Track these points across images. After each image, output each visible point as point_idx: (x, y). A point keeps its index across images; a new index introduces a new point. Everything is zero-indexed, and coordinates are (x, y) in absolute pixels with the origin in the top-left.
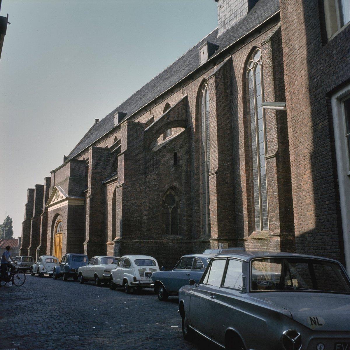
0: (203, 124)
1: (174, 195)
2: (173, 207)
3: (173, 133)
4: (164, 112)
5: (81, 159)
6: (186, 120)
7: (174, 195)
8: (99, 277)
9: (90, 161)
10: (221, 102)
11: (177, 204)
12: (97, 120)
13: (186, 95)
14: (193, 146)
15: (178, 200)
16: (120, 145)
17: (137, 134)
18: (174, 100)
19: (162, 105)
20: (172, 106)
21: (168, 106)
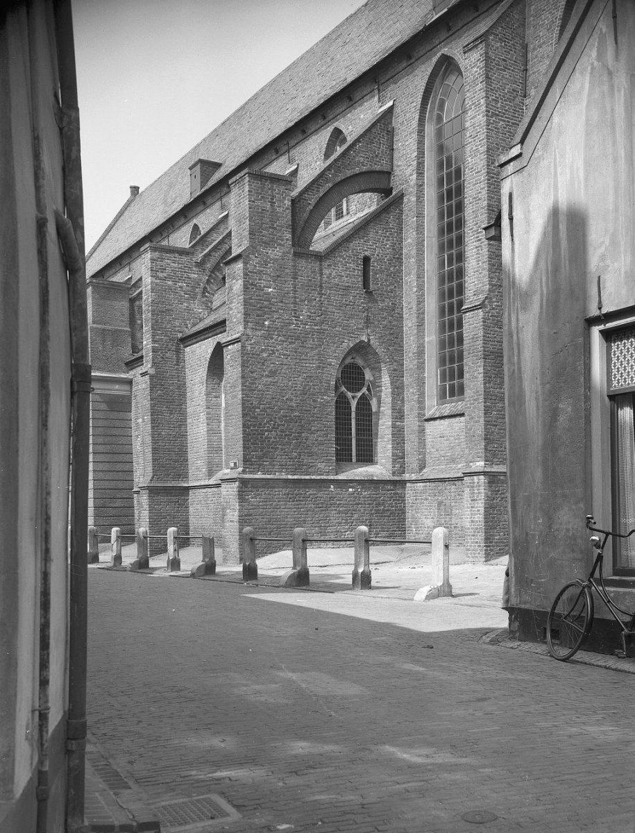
0: (618, 555)
1: (363, 367)
2: (359, 394)
3: (353, 208)
4: (327, 156)
5: (120, 277)
6: (68, 739)
7: (363, 367)
8: (193, 521)
9: (148, 280)
10: (498, 115)
11: (369, 390)
12: (135, 190)
13: (390, 103)
14: (409, 240)
15: (372, 379)
16: (140, 289)
17: (272, 203)
18: (356, 122)
19: (324, 136)
20: (350, 140)
21: (337, 135)
